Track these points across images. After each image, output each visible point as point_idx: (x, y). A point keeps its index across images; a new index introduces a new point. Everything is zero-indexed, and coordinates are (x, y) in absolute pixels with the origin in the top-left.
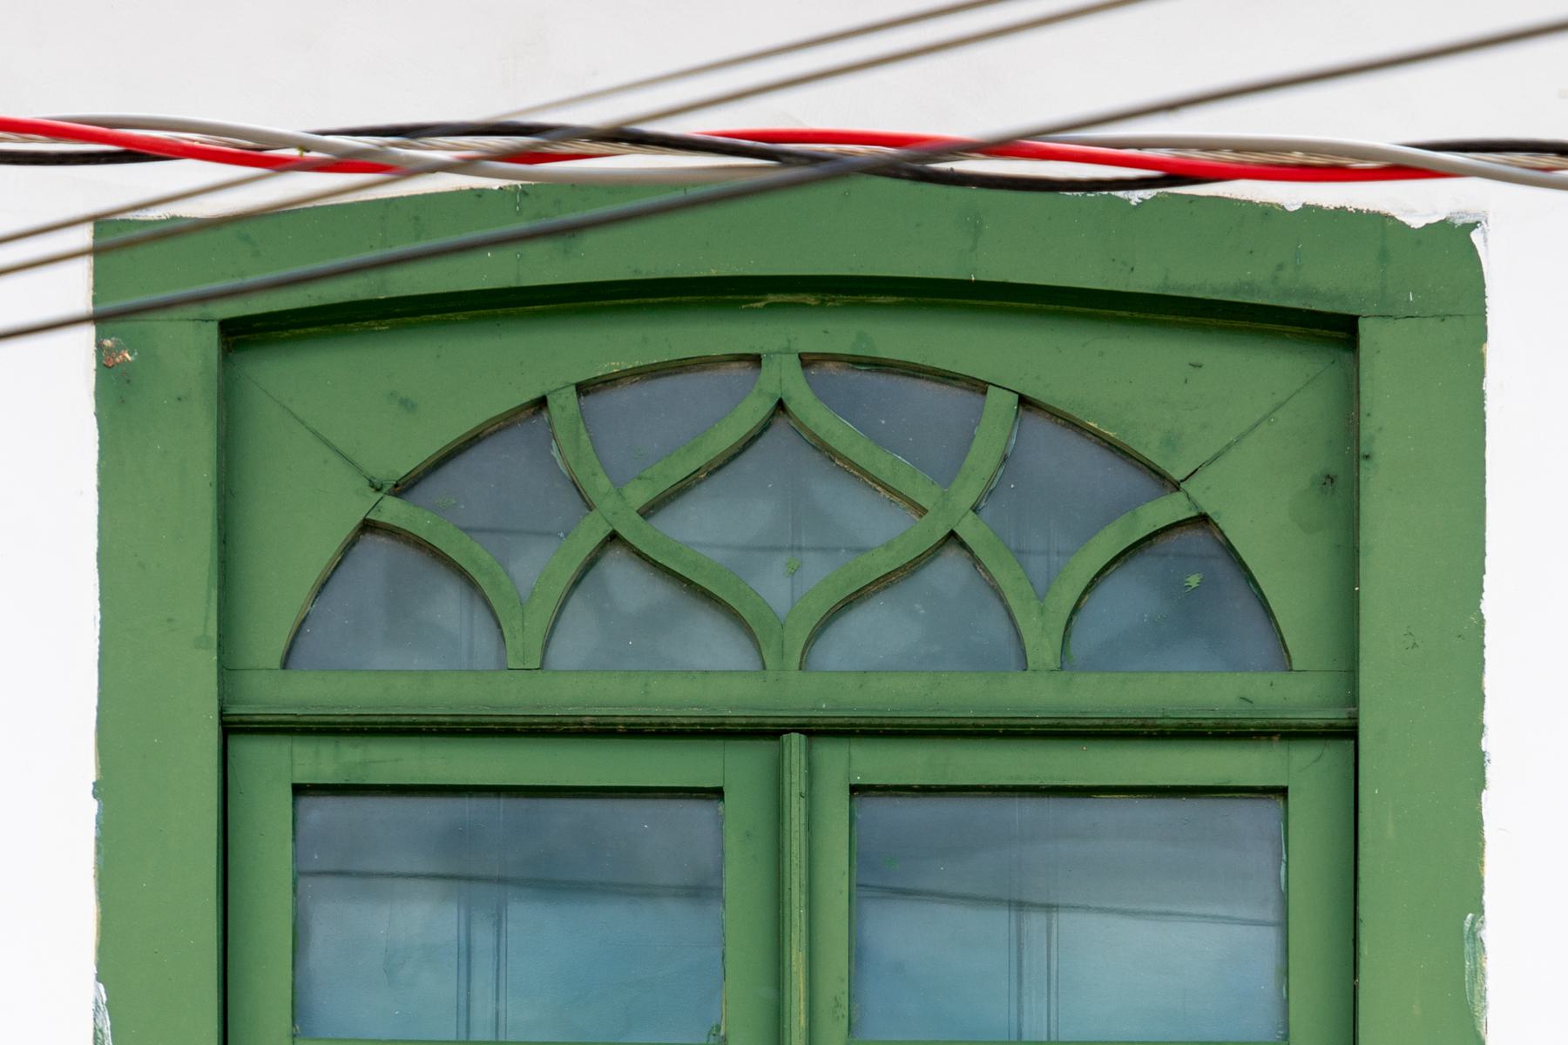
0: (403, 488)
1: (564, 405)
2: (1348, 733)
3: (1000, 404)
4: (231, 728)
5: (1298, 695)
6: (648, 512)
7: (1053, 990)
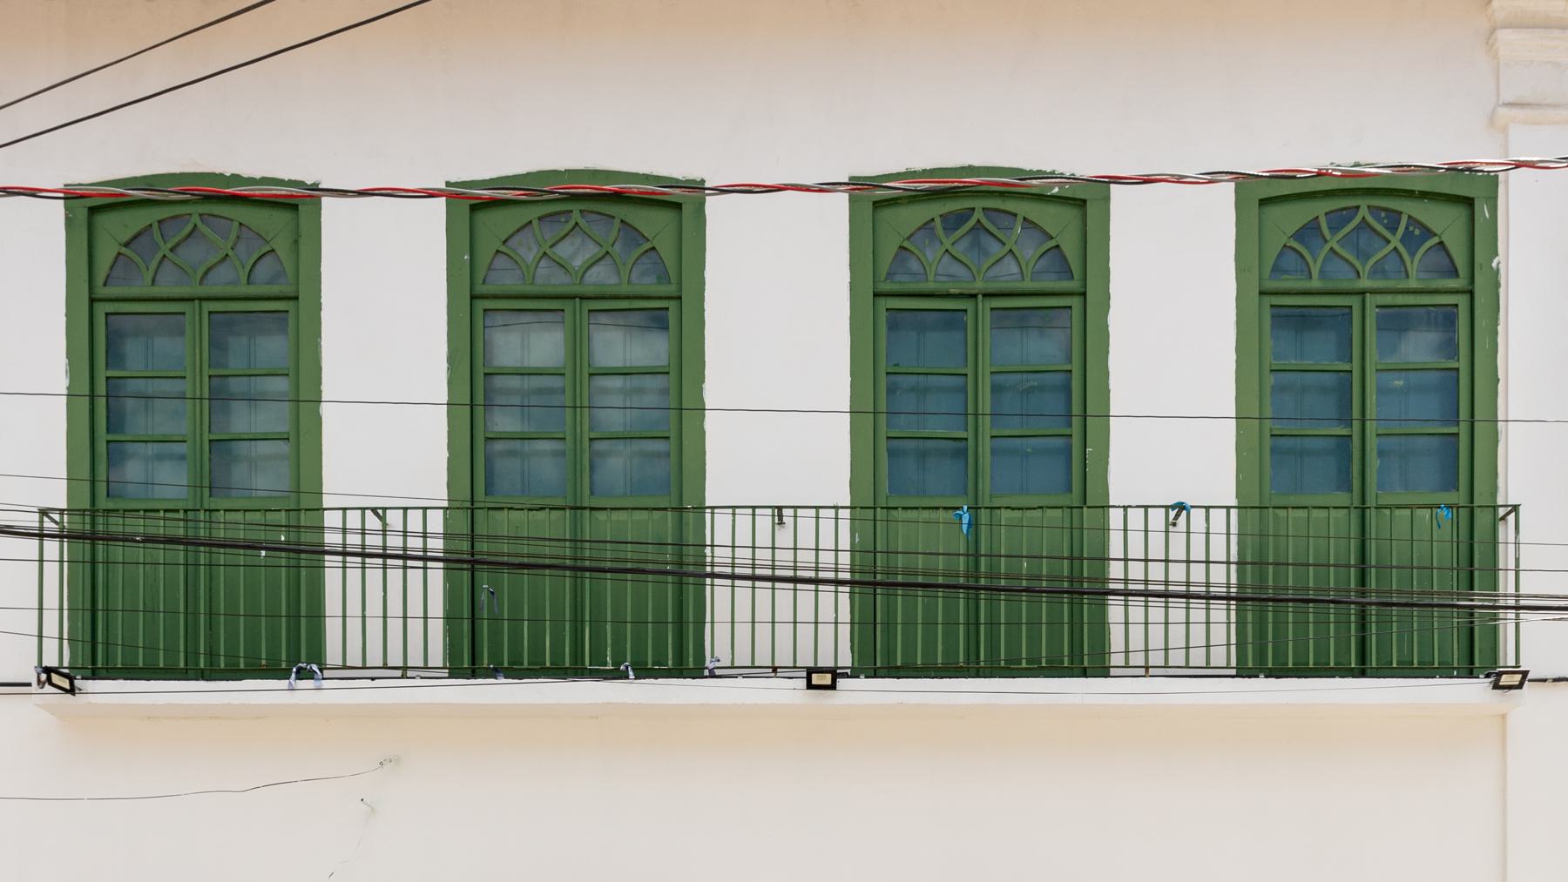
0: (126, 245)
1: (535, 222)
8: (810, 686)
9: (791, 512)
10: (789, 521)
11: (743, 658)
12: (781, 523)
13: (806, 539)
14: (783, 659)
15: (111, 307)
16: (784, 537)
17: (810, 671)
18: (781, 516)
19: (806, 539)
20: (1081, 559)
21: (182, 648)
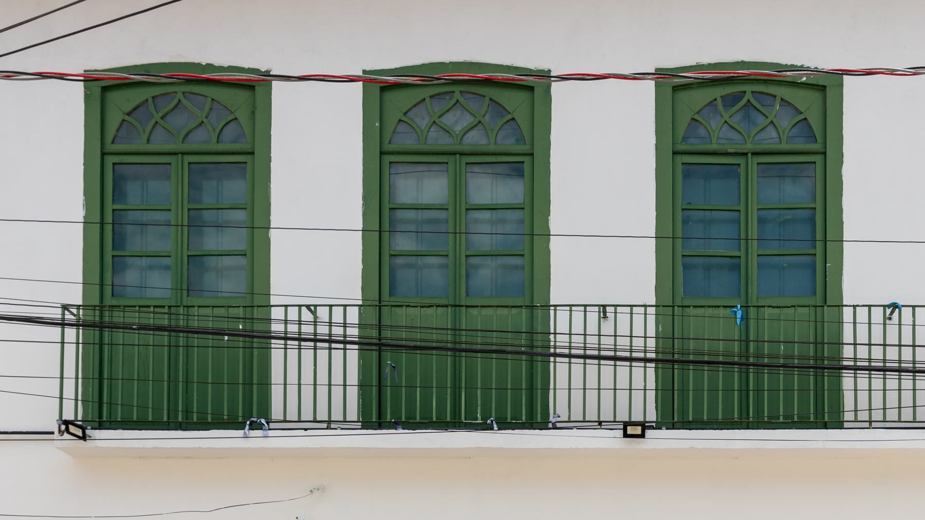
0: (129, 114)
1: (428, 100)
2: (532, 154)
3: (209, 100)
4: (382, 153)
5: (525, 148)
6: (439, 117)
7: (180, 201)
8: (626, 435)
10: (610, 316)
11: (577, 415)
12: (605, 317)
13: (624, 329)
14: (607, 416)
15: (117, 159)
17: (626, 425)
18: (605, 312)
19: (624, 329)
20: (823, 343)
21: (165, 407)
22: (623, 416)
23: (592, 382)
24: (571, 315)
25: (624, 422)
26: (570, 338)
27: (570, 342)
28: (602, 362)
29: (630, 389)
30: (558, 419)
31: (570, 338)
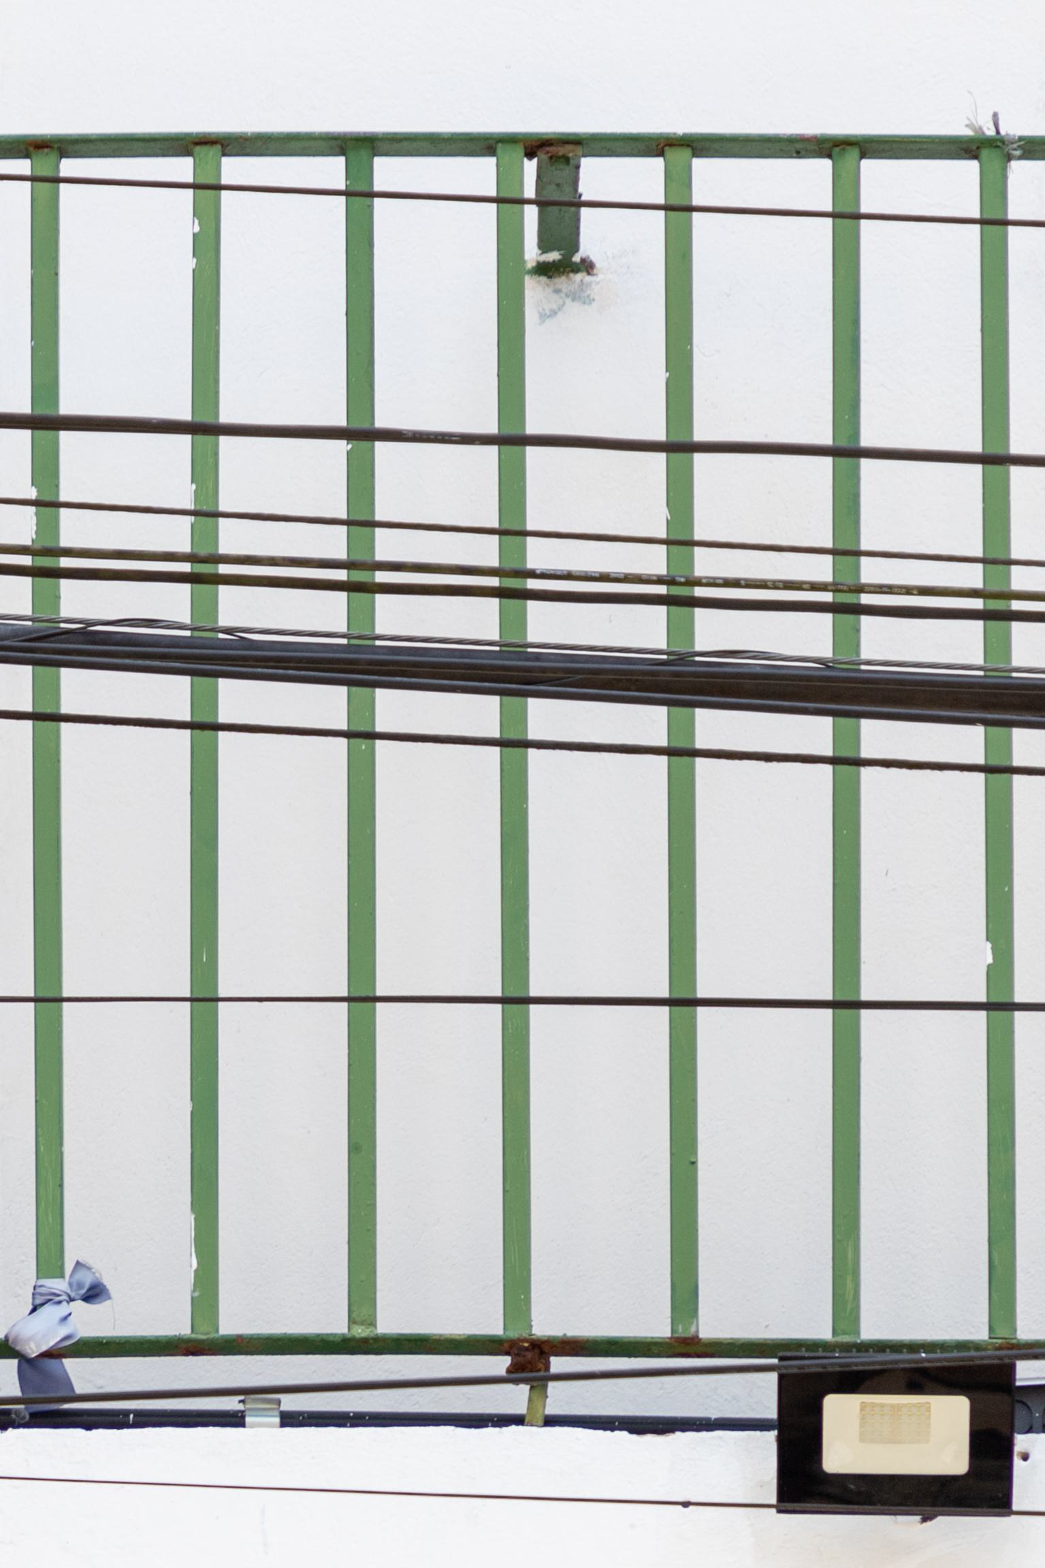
8: (804, 1482)
9: (645, 177)
10: (620, 241)
11: (441, 1281)
12: (564, 262)
13: (763, 376)
14: (598, 1283)
16: (593, 363)
17: (809, 1381)
18: (562, 209)
19: (763, 376)
22: (771, 1291)
23: (283, 928)
24: (207, 247)
25: (783, 1354)
26: (205, 472)
27: (361, 523)
28: (546, 716)
29: (362, 1000)
30: (90, 1322)
31: (205, 472)
